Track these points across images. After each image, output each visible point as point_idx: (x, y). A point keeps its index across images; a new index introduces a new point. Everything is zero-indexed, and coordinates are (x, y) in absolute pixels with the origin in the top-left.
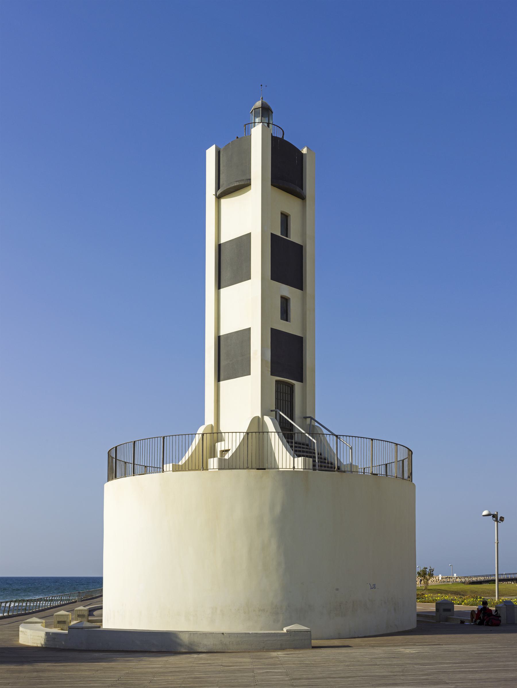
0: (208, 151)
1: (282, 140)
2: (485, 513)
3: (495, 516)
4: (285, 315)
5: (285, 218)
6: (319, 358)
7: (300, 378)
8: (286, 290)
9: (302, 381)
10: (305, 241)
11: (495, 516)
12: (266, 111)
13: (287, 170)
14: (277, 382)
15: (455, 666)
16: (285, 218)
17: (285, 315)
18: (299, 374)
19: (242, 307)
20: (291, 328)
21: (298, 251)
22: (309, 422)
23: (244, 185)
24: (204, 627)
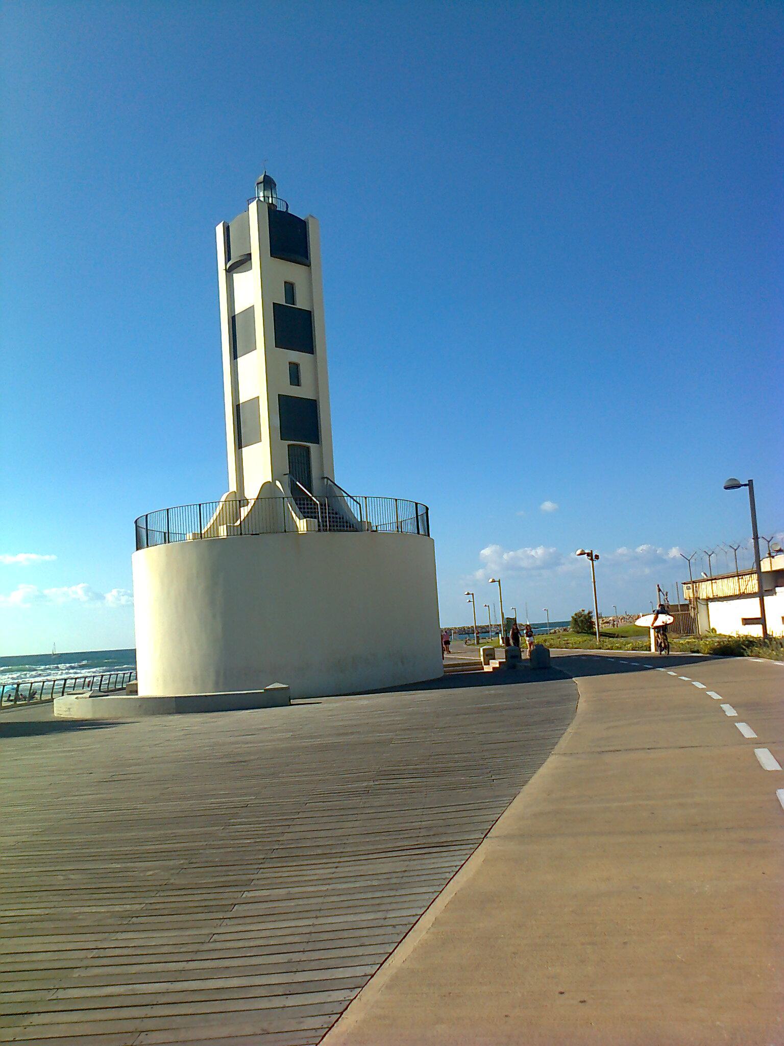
0: (217, 228)
1: (281, 208)
2: (579, 552)
3: (582, 1002)
4: (295, 379)
5: (290, 289)
6: (326, 331)
7: (316, 439)
8: (295, 356)
9: (318, 443)
11: (582, 1002)
12: (268, 183)
13: (288, 238)
14: (289, 446)
15: (221, 871)
16: (290, 289)
17: (295, 379)
18: (314, 434)
19: (253, 376)
21: (306, 317)
22: (332, 492)
23: (252, 347)
24: (106, 716)
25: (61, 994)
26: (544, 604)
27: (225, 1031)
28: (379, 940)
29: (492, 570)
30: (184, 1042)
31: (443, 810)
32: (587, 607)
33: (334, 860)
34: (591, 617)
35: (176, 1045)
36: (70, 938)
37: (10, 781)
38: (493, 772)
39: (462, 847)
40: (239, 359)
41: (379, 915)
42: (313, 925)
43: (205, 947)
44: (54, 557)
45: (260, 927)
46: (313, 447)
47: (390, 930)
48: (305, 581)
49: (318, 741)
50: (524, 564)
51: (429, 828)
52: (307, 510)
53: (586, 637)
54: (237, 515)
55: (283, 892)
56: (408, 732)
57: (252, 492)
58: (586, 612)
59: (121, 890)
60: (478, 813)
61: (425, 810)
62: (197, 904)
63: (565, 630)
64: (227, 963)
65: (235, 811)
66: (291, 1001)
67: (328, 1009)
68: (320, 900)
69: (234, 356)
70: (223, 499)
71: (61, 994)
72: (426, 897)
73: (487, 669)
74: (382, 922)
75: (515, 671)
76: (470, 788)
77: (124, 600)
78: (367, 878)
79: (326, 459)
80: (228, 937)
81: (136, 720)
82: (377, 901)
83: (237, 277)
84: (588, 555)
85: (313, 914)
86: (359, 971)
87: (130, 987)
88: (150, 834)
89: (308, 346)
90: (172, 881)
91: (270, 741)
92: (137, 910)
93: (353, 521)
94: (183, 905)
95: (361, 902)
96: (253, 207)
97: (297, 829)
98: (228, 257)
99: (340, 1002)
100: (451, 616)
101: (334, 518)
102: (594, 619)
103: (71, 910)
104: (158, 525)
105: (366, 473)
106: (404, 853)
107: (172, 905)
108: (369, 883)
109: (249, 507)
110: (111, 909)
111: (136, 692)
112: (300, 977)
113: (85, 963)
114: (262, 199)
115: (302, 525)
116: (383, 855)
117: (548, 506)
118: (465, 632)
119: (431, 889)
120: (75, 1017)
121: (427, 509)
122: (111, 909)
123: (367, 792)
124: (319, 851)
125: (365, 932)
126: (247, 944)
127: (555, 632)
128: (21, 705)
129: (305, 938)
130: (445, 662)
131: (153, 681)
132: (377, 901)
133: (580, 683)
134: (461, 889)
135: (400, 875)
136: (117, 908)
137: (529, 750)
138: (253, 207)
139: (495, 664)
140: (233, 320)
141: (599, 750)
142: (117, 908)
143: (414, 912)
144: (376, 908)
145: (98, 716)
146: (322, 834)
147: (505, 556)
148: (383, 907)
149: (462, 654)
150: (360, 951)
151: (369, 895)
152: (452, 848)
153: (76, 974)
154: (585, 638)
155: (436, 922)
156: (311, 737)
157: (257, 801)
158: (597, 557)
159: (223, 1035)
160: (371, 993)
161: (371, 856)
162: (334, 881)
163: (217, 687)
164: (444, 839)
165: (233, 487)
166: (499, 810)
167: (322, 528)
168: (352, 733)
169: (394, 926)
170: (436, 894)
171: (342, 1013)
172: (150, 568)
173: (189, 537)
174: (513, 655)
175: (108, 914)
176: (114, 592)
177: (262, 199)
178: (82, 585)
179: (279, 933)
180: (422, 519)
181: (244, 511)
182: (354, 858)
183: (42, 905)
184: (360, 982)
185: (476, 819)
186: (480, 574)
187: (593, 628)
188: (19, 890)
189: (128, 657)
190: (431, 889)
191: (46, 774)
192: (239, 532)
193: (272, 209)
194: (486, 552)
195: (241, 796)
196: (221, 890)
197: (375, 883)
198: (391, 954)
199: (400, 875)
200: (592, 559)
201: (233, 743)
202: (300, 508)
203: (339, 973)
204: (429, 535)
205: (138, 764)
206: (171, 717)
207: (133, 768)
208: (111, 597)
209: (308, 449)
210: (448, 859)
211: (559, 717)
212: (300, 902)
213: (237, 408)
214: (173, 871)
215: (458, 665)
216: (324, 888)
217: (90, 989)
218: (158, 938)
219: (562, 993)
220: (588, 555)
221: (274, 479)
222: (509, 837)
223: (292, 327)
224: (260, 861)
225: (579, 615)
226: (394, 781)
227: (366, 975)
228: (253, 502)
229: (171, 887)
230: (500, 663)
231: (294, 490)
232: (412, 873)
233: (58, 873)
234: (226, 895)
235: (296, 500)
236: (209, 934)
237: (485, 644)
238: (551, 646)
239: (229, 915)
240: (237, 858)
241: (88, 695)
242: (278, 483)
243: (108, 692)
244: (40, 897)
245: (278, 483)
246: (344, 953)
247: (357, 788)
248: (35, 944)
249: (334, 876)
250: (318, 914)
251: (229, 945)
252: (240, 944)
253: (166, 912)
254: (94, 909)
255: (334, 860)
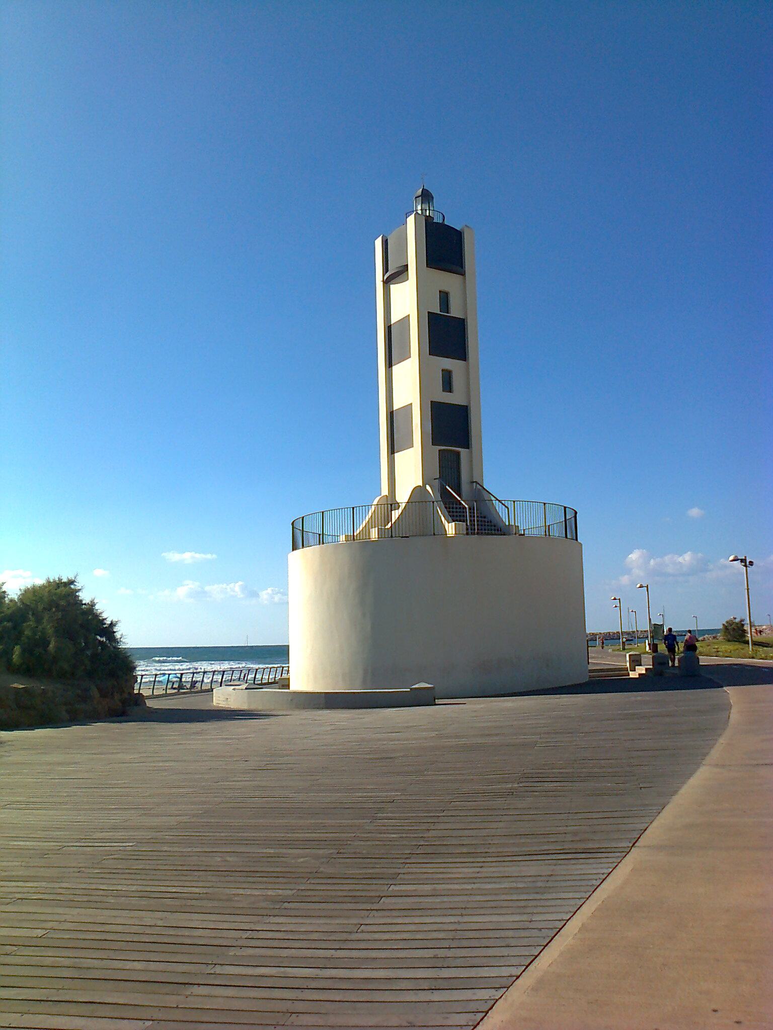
0: (376, 242)
1: (438, 219)
2: (731, 558)
3: (737, 1022)
4: (448, 385)
5: (444, 298)
6: (479, 339)
7: (467, 444)
8: (447, 363)
10: (466, 313)
11: (737, 1022)
12: (426, 196)
13: (444, 248)
16: (444, 298)
17: (448, 385)
18: (464, 439)
19: (407, 385)
20: (455, 398)
21: (461, 325)
22: (480, 496)
23: (406, 356)
25: (218, 969)
26: (693, 611)
27: (372, 1021)
28: (525, 942)
29: (641, 575)
30: (333, 1027)
31: (589, 815)
32: (739, 613)
33: (479, 860)
34: (743, 625)
35: (357, 1029)
36: (227, 917)
37: (172, 764)
38: (640, 782)
39: (610, 855)
40: (395, 368)
41: (525, 918)
42: (459, 923)
43: (354, 936)
44: (214, 556)
45: (407, 920)
46: (463, 452)
47: (535, 933)
48: (454, 582)
49: (463, 741)
50: (670, 570)
51: (575, 834)
52: (455, 514)
53: (738, 646)
54: (389, 518)
55: (428, 888)
56: (553, 736)
57: (403, 496)
58: (737, 620)
59: (275, 875)
60: (626, 821)
61: (577, 815)
62: (345, 894)
63: (714, 638)
64: (374, 954)
65: (382, 805)
66: (436, 996)
67: (473, 1006)
68: (466, 898)
69: (389, 364)
70: (375, 502)
71: (218, 969)
72: (572, 902)
73: (633, 675)
74: (528, 925)
75: (658, 679)
76: (617, 795)
77: (277, 598)
78: (513, 879)
79: (476, 464)
80: (374, 928)
81: (285, 713)
82: (522, 904)
83: (393, 287)
84: (742, 561)
85: (458, 912)
86: (505, 971)
87: (282, 969)
88: (301, 822)
89: (461, 353)
90: (321, 869)
91: (415, 739)
92: (288, 896)
93: (502, 525)
94: (334, 893)
95: (505, 904)
96: (411, 220)
97: (442, 826)
98: (386, 269)
99: (486, 1001)
100: (599, 618)
101: (483, 522)
102: (747, 628)
103: (228, 891)
104: (313, 526)
105: (514, 477)
106: (549, 857)
107: (321, 893)
108: (514, 885)
109: (400, 510)
110: (265, 892)
111: (288, 686)
112: (445, 973)
113: (240, 943)
114: (420, 212)
115: (450, 528)
116: (527, 858)
117: (695, 512)
118: (610, 638)
119: (578, 895)
120: (230, 992)
121: (576, 513)
122: (265, 892)
123: (511, 793)
124: (465, 850)
125: (510, 933)
126: (394, 936)
127: (704, 640)
128: (184, 693)
129: (451, 935)
130: (591, 667)
131: (303, 676)
132: (522, 904)
133: (732, 693)
134: (609, 897)
135: (546, 878)
136: (270, 893)
137: (683, 761)
138: (411, 220)
139: (641, 670)
140: (389, 329)
141: (756, 762)
142: (270, 893)
143: (559, 917)
144: (522, 910)
145: (253, 707)
146: (466, 833)
147: (652, 562)
148: (529, 910)
149: (604, 659)
150: (505, 951)
151: (515, 897)
152: (600, 855)
153: (232, 952)
154: (736, 647)
155: (584, 928)
156: (457, 737)
157: (403, 797)
158: (751, 563)
159: (370, 1024)
160: (517, 994)
161: (535, 857)
162: (478, 880)
163: (364, 684)
164: (590, 846)
165: (385, 491)
166: (647, 819)
167: (470, 531)
168: (497, 735)
169: (540, 929)
170: (583, 901)
171: (487, 1012)
172: (303, 566)
173: (342, 538)
174: (659, 662)
175: (261, 898)
176: (269, 590)
177: (420, 212)
178: (240, 583)
179: (426, 928)
180: (570, 523)
181: (395, 514)
182: (499, 859)
183: (201, 884)
184: (505, 982)
185: (623, 827)
186: (625, 580)
187: (745, 636)
188: (180, 868)
189: (281, 653)
190: (578, 895)
191: (206, 759)
192: (388, 535)
193: (429, 221)
194: (634, 556)
195: (387, 791)
196: (369, 882)
197: (520, 885)
198: (536, 957)
199: (546, 878)
200: (746, 566)
201: (379, 740)
202: (449, 512)
203: (485, 972)
204: (577, 539)
205: (290, 755)
206: (320, 712)
207: (286, 758)
208: (265, 595)
209: (458, 454)
210: (594, 866)
211: (710, 727)
212: (445, 899)
213: (391, 415)
214: (323, 860)
215: (602, 670)
216: (469, 887)
217: (250, 968)
218: (307, 925)
219: (715, 1011)
220: (742, 561)
221: (424, 484)
222: (659, 848)
223: (446, 335)
224: (406, 856)
225: (730, 623)
226: (539, 784)
227: (511, 976)
228: (404, 505)
229: (319, 875)
230: (646, 669)
231: (445, 495)
232: (558, 878)
233: (214, 854)
234: (374, 887)
235: (445, 504)
236: (356, 925)
237: (631, 650)
238: (701, 654)
239: (375, 907)
240: (383, 851)
241: (245, 686)
242: (428, 488)
243: (263, 685)
244: (199, 876)
245: (428, 488)
246: (490, 952)
247: (502, 788)
248: (196, 920)
249: (479, 875)
250: (464, 912)
251: (377, 936)
252: (387, 936)
253: (316, 899)
254: (249, 892)
255: (479, 860)
